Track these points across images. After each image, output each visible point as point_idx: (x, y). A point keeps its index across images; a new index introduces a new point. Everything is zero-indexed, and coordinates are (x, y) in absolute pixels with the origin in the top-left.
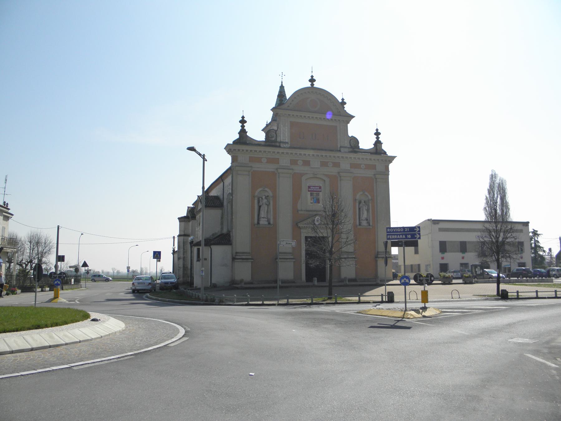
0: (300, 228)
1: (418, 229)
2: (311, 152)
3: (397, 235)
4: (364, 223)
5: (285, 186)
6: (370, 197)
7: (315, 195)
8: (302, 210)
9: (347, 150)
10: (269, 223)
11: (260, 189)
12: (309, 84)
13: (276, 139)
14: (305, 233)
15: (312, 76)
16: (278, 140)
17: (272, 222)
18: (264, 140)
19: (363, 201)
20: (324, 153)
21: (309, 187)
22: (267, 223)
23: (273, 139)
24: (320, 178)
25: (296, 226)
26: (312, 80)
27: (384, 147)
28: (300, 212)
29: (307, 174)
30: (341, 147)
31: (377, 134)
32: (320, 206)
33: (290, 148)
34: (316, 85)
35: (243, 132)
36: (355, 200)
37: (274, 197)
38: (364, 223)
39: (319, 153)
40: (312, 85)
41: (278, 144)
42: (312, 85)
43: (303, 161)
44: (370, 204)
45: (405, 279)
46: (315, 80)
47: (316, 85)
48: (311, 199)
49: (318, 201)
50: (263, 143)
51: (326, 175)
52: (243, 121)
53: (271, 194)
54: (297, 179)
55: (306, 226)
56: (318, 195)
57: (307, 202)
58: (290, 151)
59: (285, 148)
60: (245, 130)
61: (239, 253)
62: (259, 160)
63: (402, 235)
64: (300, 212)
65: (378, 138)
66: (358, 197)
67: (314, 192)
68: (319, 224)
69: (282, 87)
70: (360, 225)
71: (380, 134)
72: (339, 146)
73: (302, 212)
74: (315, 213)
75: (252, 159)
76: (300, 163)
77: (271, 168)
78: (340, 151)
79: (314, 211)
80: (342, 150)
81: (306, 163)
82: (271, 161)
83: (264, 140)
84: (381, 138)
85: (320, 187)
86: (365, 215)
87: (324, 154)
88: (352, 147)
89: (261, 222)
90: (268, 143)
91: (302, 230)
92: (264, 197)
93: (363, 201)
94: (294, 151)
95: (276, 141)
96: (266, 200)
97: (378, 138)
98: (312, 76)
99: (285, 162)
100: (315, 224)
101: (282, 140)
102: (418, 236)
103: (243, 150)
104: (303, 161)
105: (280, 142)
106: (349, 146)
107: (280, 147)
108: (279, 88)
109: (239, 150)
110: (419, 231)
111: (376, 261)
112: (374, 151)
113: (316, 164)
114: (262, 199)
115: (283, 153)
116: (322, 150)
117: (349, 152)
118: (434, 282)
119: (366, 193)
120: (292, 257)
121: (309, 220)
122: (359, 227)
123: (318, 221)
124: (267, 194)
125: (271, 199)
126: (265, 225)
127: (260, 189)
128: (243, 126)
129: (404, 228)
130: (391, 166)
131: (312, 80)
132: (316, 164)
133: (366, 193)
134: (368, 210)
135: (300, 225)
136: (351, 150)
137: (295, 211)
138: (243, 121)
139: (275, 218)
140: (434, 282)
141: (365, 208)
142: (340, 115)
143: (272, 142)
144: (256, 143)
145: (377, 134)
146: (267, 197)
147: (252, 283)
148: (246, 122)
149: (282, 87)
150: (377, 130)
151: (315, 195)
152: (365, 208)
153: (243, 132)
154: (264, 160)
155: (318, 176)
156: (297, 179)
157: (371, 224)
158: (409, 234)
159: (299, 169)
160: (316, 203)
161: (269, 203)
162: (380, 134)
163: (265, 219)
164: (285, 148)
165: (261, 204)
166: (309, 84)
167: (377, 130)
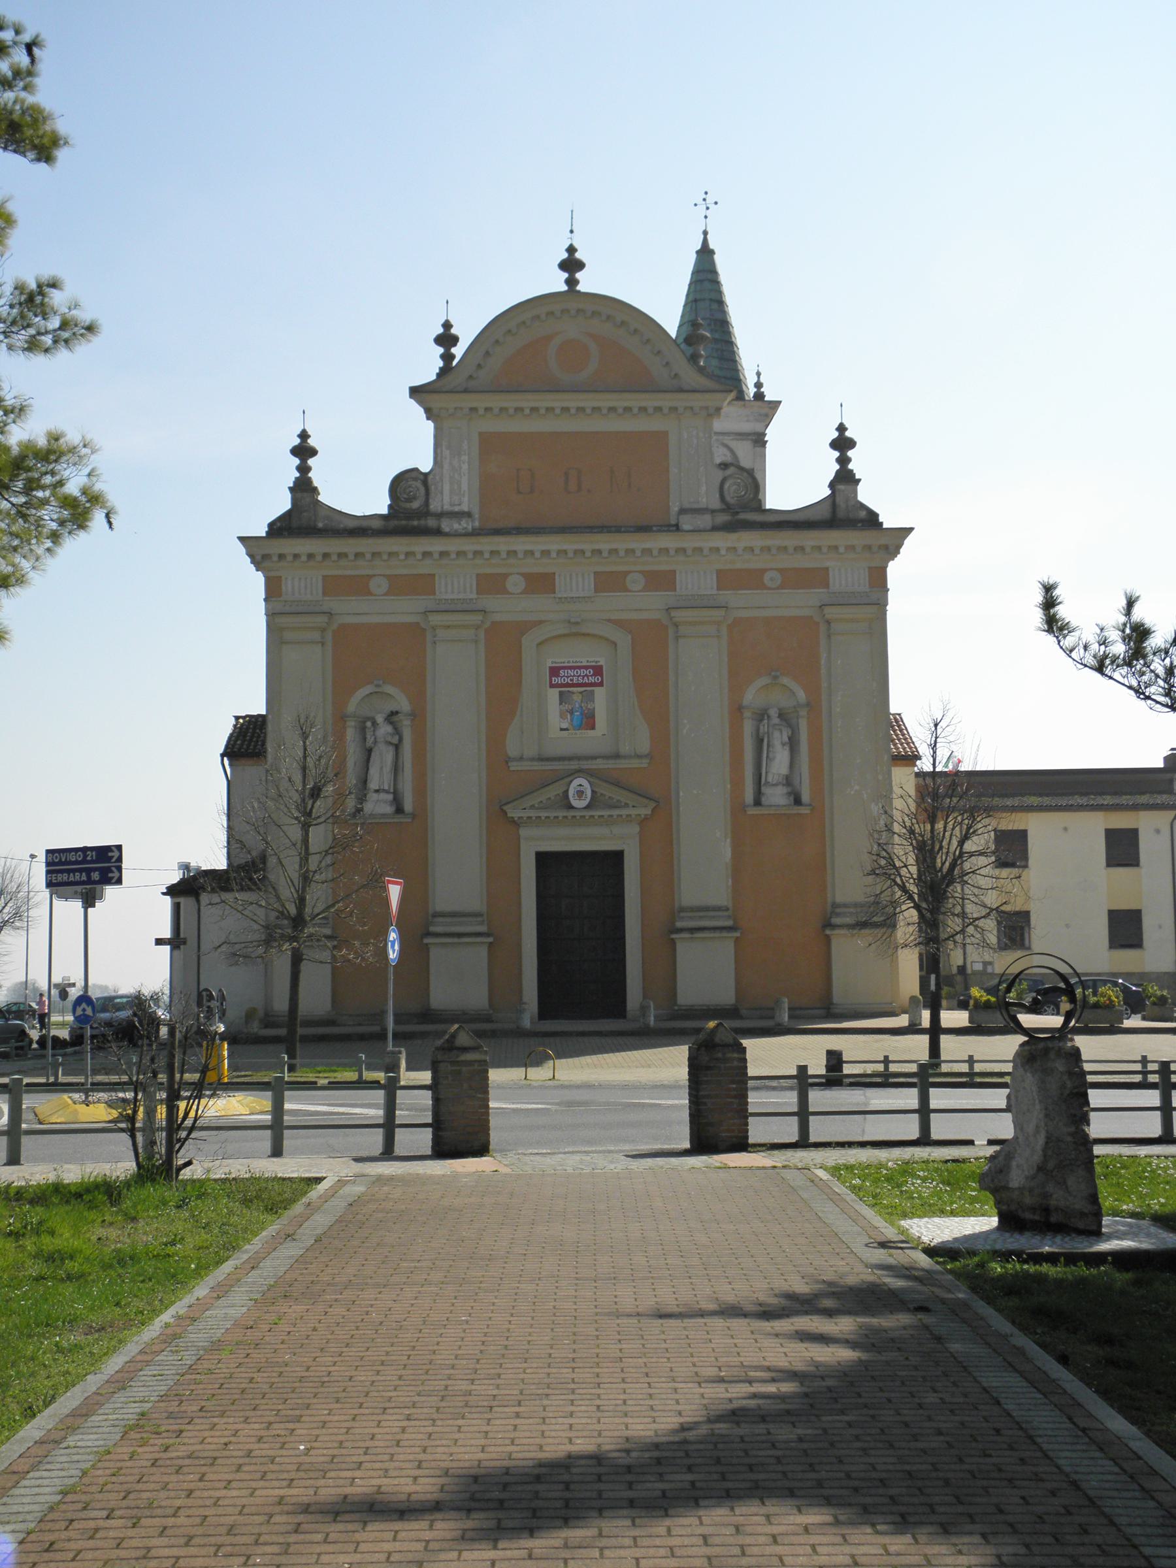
0: (516, 823)
1: (116, 854)
2: (554, 543)
3: (69, 871)
4: (776, 796)
5: (456, 674)
6: (801, 695)
7: (577, 698)
8: (521, 759)
9: (706, 520)
10: (399, 810)
11: (368, 689)
12: (557, 282)
13: (427, 503)
14: (538, 839)
15: (571, 250)
16: (435, 506)
17: (408, 806)
18: (385, 511)
19: (773, 713)
20: (604, 543)
21: (554, 671)
22: (389, 809)
23: (415, 505)
24: (601, 637)
25: (500, 818)
26: (572, 265)
27: (866, 495)
28: (514, 766)
29: (541, 622)
30: (683, 511)
31: (842, 443)
32: (597, 738)
33: (475, 533)
34: (587, 282)
35: (303, 487)
36: (737, 710)
37: (418, 715)
38: (776, 796)
39: (588, 543)
40: (572, 282)
41: (431, 523)
42: (572, 282)
43: (528, 577)
44: (803, 725)
45: (84, 1005)
46: (580, 265)
47: (587, 282)
48: (562, 716)
49: (589, 721)
50: (377, 524)
51: (619, 623)
52: (304, 451)
53: (403, 703)
54: (503, 646)
55: (533, 814)
56: (590, 697)
57: (549, 724)
58: (469, 545)
59: (457, 535)
60: (309, 481)
61: (839, 906)
62: (359, 587)
63: (80, 871)
64: (514, 766)
65: (843, 461)
66: (751, 696)
67: (574, 685)
68: (588, 807)
69: (705, 254)
70: (757, 803)
71: (851, 444)
72: (675, 509)
73: (525, 766)
74: (574, 765)
75: (333, 586)
76: (515, 584)
77: (403, 610)
78: (677, 528)
79: (570, 759)
80: (687, 523)
81: (541, 583)
82: (401, 586)
83: (385, 511)
84: (858, 462)
85: (598, 670)
86: (779, 763)
87: (602, 546)
88: (727, 508)
89: (368, 807)
90: (394, 523)
91: (523, 832)
92: (380, 719)
93: (773, 713)
94: (487, 544)
95: (425, 512)
96: (389, 729)
97: (843, 461)
98: (571, 250)
99: (457, 584)
100: (571, 807)
101: (447, 507)
102: (116, 875)
103: (296, 556)
104: (523, 575)
105: (441, 515)
106: (716, 504)
107: (438, 532)
108: (693, 258)
109: (281, 557)
110: (120, 859)
111: (828, 939)
112: (825, 513)
113: (576, 582)
114: (374, 723)
115: (443, 554)
116: (591, 529)
117: (715, 528)
118: (1128, 1023)
119: (785, 681)
120: (483, 929)
121: (553, 792)
122: (753, 811)
123: (580, 794)
124: (393, 707)
125: (407, 722)
126: (384, 815)
127: (368, 689)
128: (304, 469)
129: (85, 850)
130: (894, 569)
131: (572, 265)
132: (576, 582)
133: (785, 681)
134: (793, 744)
135: (514, 813)
136: (723, 518)
137: (497, 758)
138: (304, 451)
139: (421, 791)
140: (1128, 1023)
141: (779, 738)
142: (681, 390)
143: (411, 515)
144: (351, 524)
145: (842, 443)
146: (391, 717)
147: (331, 1022)
148: (313, 452)
149: (705, 254)
150: (841, 428)
151: (577, 698)
152: (779, 738)
153: (303, 487)
154: (379, 586)
155: (584, 630)
156: (503, 646)
157: (805, 798)
158: (95, 869)
159: (511, 607)
160: (580, 728)
161: (401, 740)
162: (851, 444)
163: (383, 796)
164: (457, 535)
165: (370, 740)
166: (557, 282)
167: (841, 428)
